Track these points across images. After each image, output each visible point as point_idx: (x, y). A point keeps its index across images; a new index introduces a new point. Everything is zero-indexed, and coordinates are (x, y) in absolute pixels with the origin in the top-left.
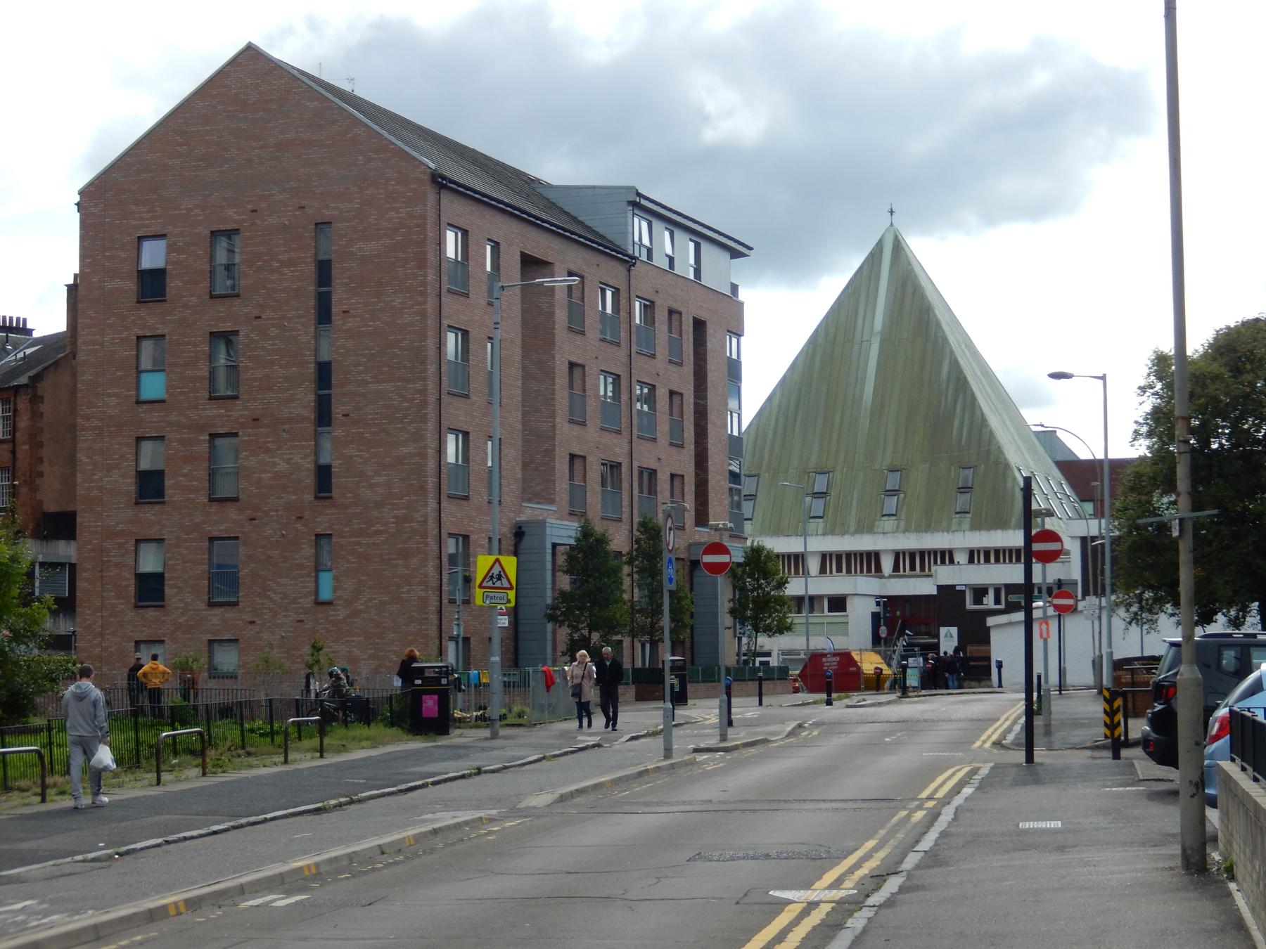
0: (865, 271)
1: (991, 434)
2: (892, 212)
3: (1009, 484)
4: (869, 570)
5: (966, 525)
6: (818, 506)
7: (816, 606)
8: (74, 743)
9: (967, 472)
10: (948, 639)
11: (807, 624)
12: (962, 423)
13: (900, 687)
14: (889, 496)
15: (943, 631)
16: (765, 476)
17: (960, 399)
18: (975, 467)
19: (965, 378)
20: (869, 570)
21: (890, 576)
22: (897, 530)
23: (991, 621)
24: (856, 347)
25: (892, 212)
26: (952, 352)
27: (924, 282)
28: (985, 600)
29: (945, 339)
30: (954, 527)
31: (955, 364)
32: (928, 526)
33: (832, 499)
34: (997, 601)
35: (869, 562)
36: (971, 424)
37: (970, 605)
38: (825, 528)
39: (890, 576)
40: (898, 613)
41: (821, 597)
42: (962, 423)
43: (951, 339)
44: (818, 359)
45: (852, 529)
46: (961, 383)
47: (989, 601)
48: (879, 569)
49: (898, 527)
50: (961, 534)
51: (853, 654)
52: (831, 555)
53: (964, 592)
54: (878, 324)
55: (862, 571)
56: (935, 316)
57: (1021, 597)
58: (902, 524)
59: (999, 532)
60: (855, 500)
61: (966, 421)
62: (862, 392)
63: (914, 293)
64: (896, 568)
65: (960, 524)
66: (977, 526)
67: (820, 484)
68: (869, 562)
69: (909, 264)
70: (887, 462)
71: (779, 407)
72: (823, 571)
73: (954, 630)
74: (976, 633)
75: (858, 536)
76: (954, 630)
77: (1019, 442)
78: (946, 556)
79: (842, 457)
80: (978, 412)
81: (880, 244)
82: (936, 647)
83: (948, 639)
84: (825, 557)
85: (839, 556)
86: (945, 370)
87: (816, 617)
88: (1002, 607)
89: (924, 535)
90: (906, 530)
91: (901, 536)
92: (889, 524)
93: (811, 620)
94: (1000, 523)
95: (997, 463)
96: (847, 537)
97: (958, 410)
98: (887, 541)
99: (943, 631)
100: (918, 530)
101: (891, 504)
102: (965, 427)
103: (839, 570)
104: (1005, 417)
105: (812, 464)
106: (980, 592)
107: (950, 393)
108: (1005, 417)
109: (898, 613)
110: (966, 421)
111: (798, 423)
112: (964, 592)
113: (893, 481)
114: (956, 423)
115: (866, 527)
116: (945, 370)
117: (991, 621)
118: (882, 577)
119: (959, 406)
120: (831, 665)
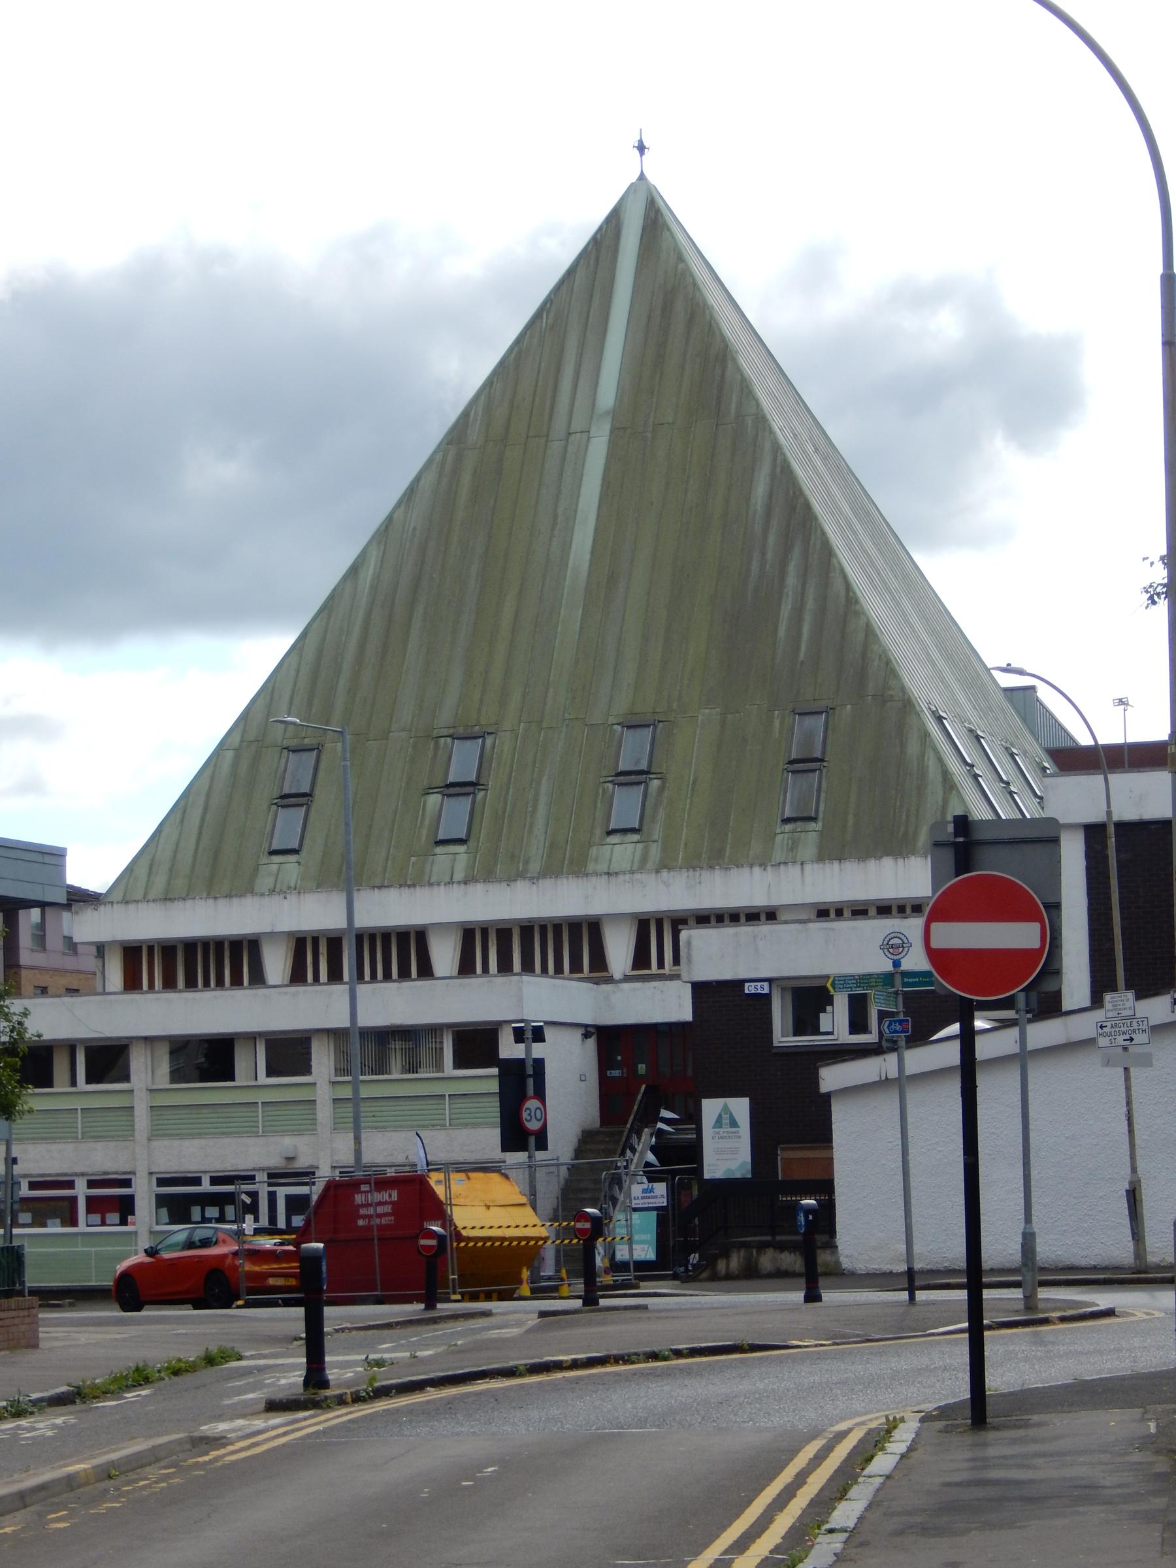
0: (580, 275)
1: (870, 632)
2: (641, 148)
3: (913, 748)
4: (576, 967)
5: (809, 848)
6: (454, 815)
7: (424, 1054)
8: (255, 1234)
9: (809, 721)
10: (726, 1140)
11: (356, 1101)
12: (798, 611)
13: (584, 1266)
14: (627, 789)
15: (711, 1108)
16: (334, 748)
17: (796, 553)
18: (828, 711)
19: (808, 506)
20: (576, 967)
21: (627, 979)
22: (642, 866)
23: (831, 1077)
24: (556, 447)
25: (641, 148)
26: (777, 448)
27: (713, 298)
28: (825, 1021)
29: (761, 420)
30: (778, 855)
31: (784, 476)
32: (716, 853)
33: (488, 798)
34: (858, 1024)
35: (573, 945)
36: (822, 611)
37: (782, 1036)
38: (471, 866)
39: (627, 979)
40: (642, 1068)
41: (435, 1030)
42: (798, 611)
43: (777, 423)
44: (466, 478)
45: (535, 867)
46: (796, 517)
47: (835, 1022)
48: (599, 962)
49: (644, 859)
50: (794, 871)
51: (434, 1179)
52: (485, 932)
53: (767, 998)
54: (607, 395)
55: (559, 970)
56: (738, 369)
57: (926, 1006)
58: (655, 851)
59: (888, 862)
60: (543, 800)
61: (810, 604)
62: (566, 546)
63: (691, 321)
64: (641, 959)
65: (793, 846)
66: (833, 851)
67: (462, 763)
68: (573, 945)
69: (680, 258)
70: (622, 704)
71: (374, 588)
72: (466, 967)
73: (740, 1107)
74: (795, 1118)
75: (547, 883)
76: (740, 1107)
77: (941, 663)
78: (404, 952)
79: (516, 697)
80: (838, 583)
81: (614, 220)
82: (693, 1152)
83: (726, 1140)
84: (471, 937)
85: (504, 933)
86: (760, 490)
87: (424, 1083)
88: (870, 1038)
89: (706, 875)
90: (665, 865)
91: (650, 879)
92: (623, 851)
93: (365, 1092)
94: (889, 843)
95: (882, 699)
96: (521, 885)
97: (791, 580)
98: (614, 893)
99: (711, 1108)
100: (693, 864)
101: (626, 805)
102: (808, 618)
103: (505, 967)
104: (907, 605)
105: (445, 717)
106: (810, 999)
107: (772, 539)
108: (907, 605)
109: (642, 1068)
110: (810, 604)
111: (417, 624)
112: (767, 998)
113: (633, 751)
114: (786, 609)
115: (568, 862)
116: (760, 490)
117: (831, 1077)
118: (610, 980)
119: (792, 568)
120: (375, 1207)
